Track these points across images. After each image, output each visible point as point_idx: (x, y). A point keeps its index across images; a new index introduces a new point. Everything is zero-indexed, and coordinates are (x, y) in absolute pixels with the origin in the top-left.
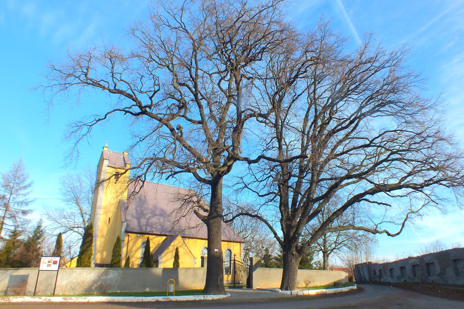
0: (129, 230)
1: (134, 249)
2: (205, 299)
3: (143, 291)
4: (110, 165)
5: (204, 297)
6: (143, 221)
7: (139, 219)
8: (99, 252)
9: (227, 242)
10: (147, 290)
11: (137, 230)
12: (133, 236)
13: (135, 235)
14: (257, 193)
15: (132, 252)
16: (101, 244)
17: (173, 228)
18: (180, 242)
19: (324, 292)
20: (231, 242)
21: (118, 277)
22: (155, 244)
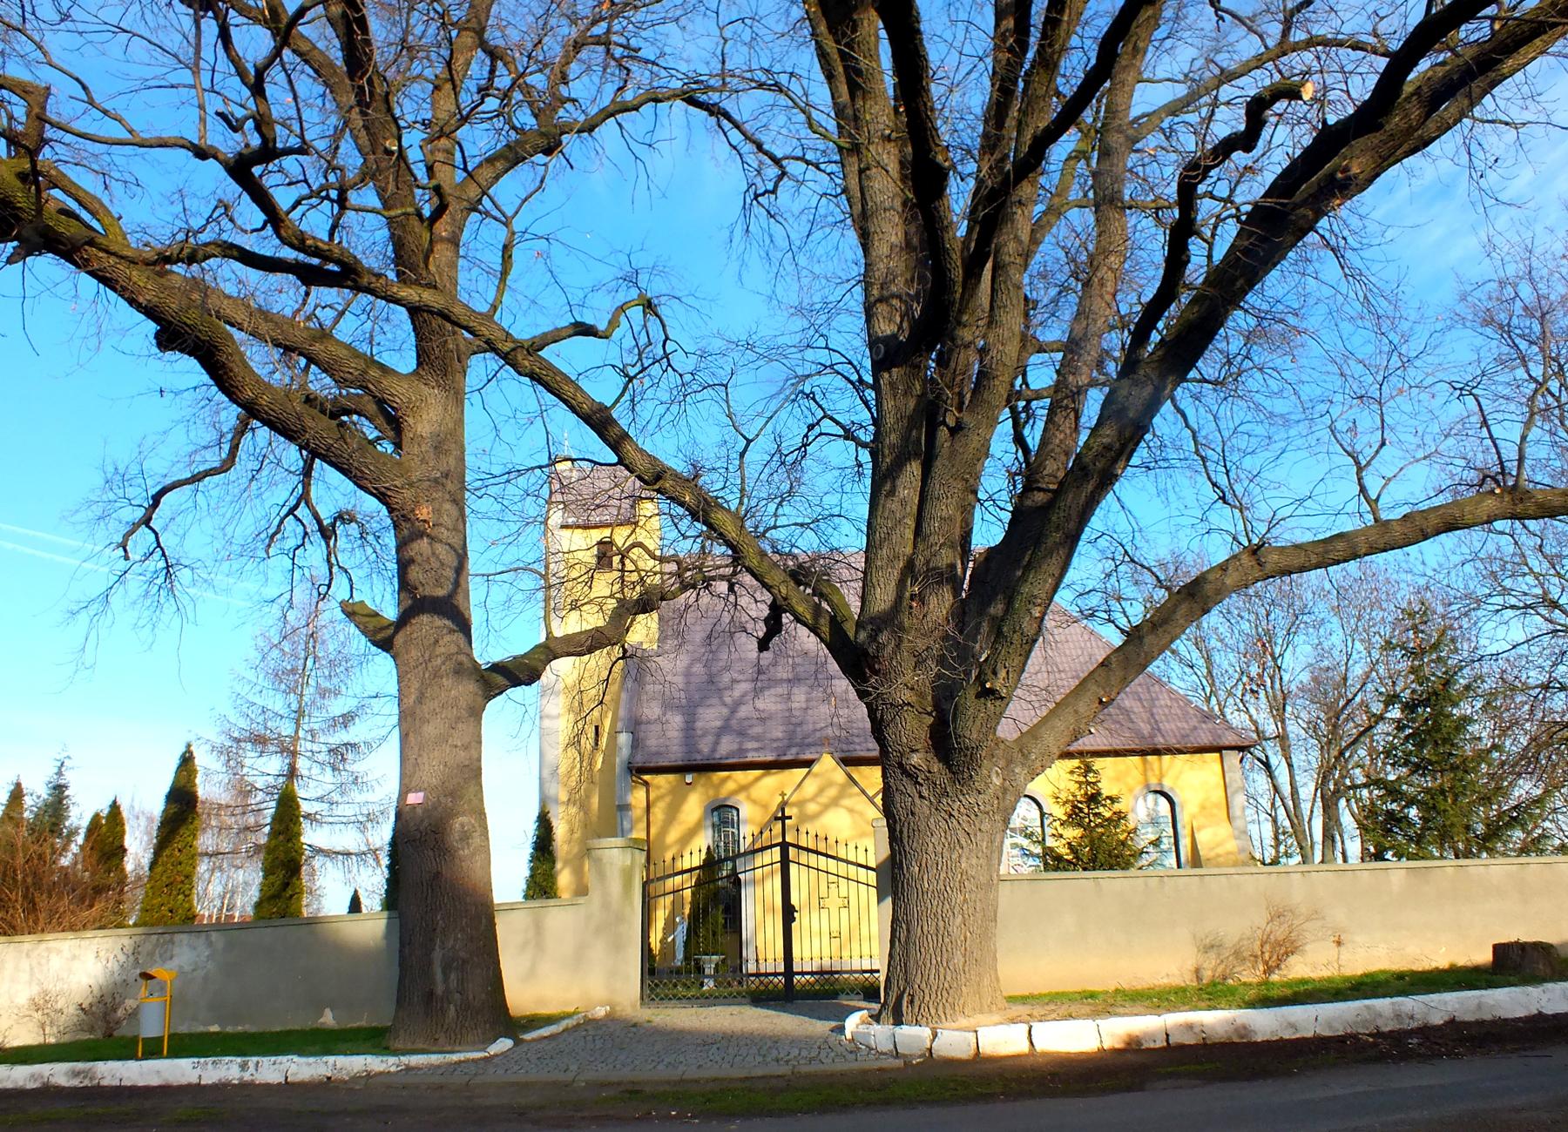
0: (639, 760)
1: (673, 835)
2: (247, 1077)
3: (309, 1025)
4: (571, 521)
5: (244, 1067)
6: (710, 717)
7: (690, 713)
8: (566, 863)
9: (1136, 759)
10: (328, 1019)
11: (676, 755)
12: (662, 781)
13: (671, 777)
14: (1357, 463)
15: (666, 848)
16: (572, 831)
17: (649, 722)
18: (830, 784)
19: (1220, 1034)
20: (1157, 752)
21: (210, 965)
22: (765, 807)
